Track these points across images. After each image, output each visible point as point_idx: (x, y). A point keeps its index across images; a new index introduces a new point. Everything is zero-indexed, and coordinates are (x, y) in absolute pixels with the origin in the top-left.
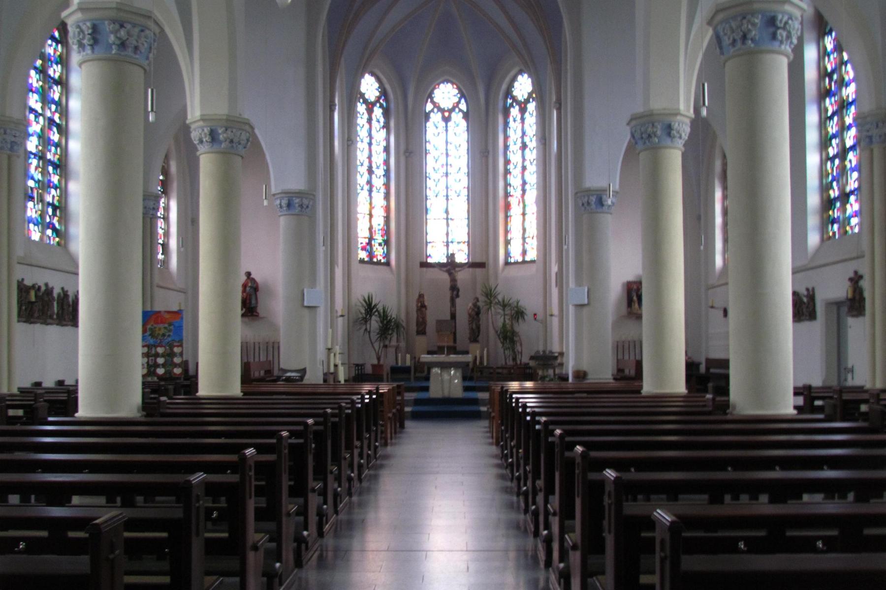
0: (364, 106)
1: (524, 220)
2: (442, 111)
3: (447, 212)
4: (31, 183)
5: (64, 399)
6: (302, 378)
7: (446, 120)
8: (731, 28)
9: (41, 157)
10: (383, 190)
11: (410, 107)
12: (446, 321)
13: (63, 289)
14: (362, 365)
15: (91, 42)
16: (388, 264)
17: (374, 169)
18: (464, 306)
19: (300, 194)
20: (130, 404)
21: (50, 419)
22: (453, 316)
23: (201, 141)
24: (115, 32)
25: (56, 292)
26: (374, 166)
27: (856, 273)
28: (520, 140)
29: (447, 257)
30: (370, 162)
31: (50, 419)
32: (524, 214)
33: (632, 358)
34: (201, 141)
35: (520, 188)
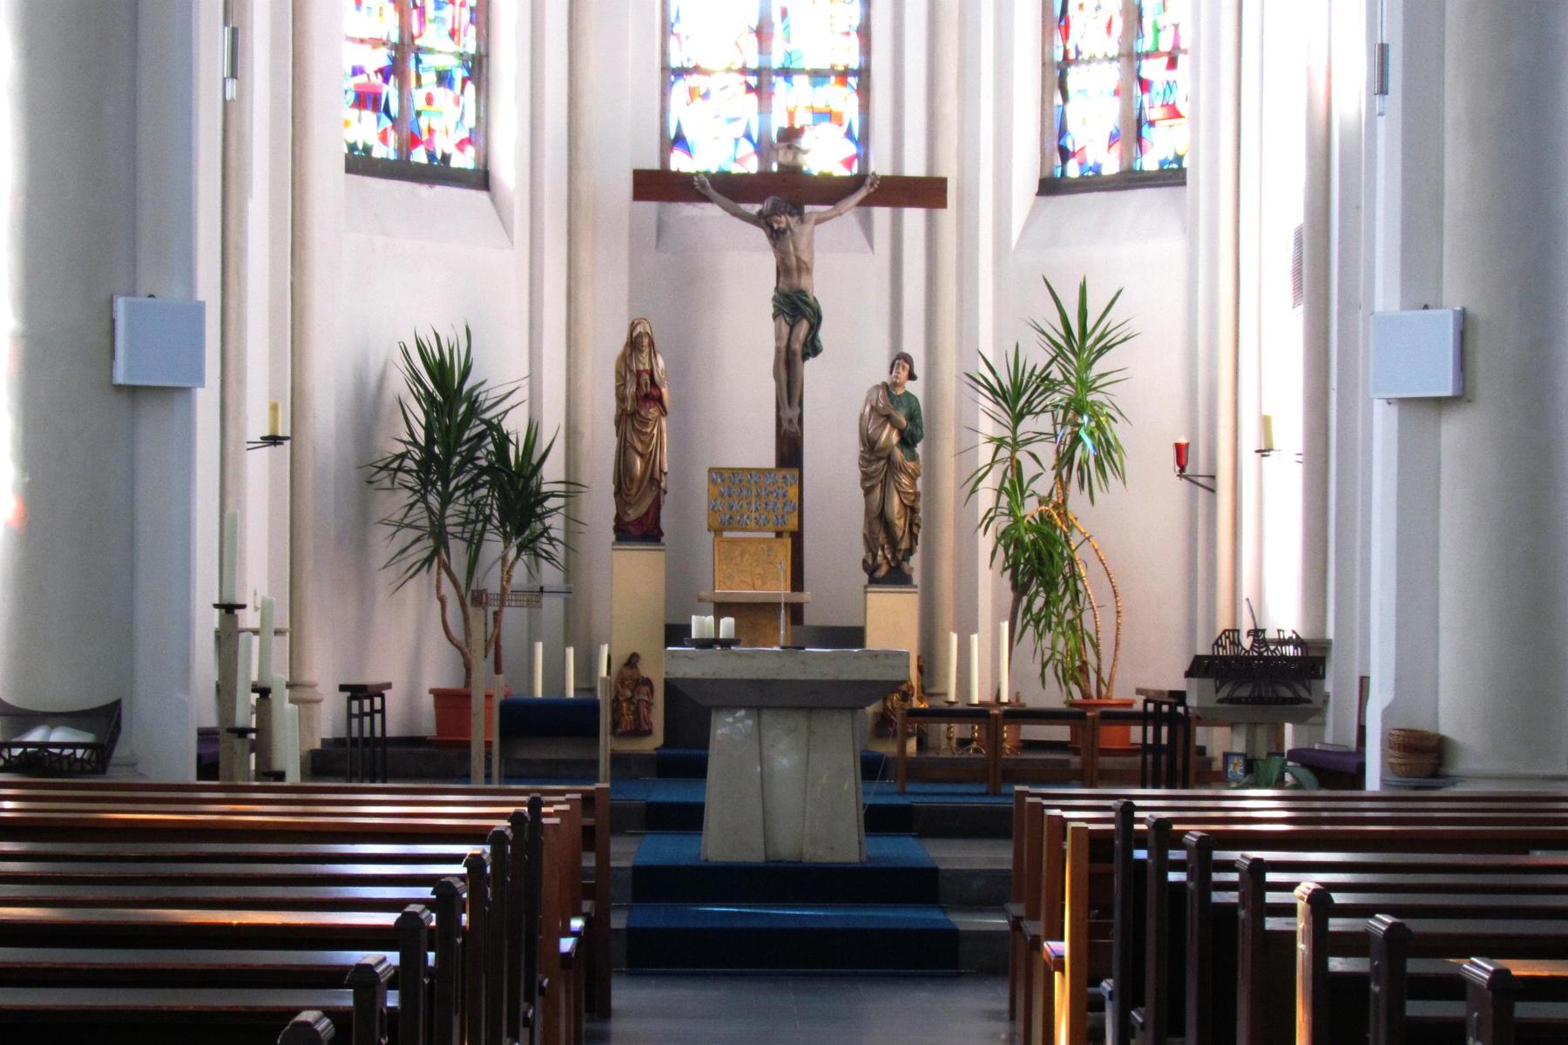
6: (102, 753)
12: (769, 471)
14: (377, 691)
16: (481, 179)
22: (790, 450)
29: (763, 149)
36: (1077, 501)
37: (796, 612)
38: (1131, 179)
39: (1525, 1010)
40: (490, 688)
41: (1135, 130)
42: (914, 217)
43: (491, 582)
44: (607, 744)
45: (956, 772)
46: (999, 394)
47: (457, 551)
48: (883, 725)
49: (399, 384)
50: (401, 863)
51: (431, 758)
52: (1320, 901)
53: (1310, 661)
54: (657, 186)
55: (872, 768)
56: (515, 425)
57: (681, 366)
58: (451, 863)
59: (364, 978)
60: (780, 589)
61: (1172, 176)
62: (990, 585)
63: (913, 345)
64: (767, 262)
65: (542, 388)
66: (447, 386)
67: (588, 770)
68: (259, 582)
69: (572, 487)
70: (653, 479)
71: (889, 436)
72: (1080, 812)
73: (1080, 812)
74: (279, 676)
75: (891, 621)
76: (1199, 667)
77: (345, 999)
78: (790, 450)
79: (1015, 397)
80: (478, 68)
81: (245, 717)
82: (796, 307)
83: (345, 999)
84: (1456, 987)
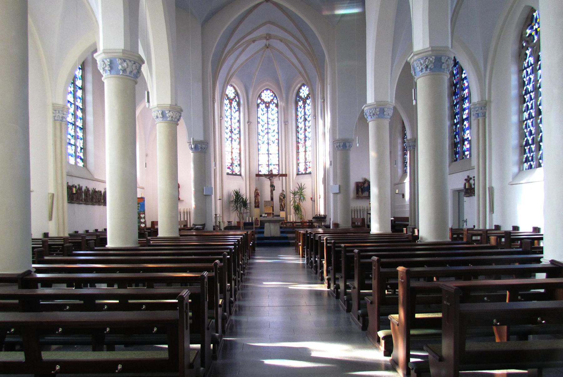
0: (228, 101)
1: (305, 154)
2: (265, 103)
3: (268, 150)
4: (69, 137)
5: (100, 238)
6: (203, 228)
7: (267, 107)
8: (421, 63)
9: (74, 124)
10: (238, 140)
11: (250, 101)
13: (87, 187)
15: (109, 69)
16: (240, 175)
17: (233, 130)
18: (277, 194)
19: (201, 142)
20: (131, 242)
21: (96, 248)
22: (272, 199)
23: (157, 117)
24: (121, 64)
25: (84, 188)
26: (233, 129)
27: (468, 176)
28: (303, 117)
29: (269, 172)
30: (231, 127)
31: (96, 248)
32: (305, 151)
33: (359, 217)
34: (157, 117)
35: (303, 139)
36: (301, 203)
37: (273, 214)
38: (306, 174)
39: (347, 249)
40: (242, 221)
41: (306, 169)
42: (284, 178)
43: (242, 211)
44: (254, 226)
45: (289, 228)
46: (293, 193)
47: (239, 209)
48: (282, 224)
49: (232, 194)
50: (234, 237)
51: (237, 228)
52: (326, 239)
53: (325, 217)
54: (258, 175)
55: (281, 228)
56: (244, 197)
57: (261, 191)
58: (239, 238)
59: (230, 249)
60: (272, 212)
61: (310, 173)
62: (292, 211)
63: (284, 189)
64: (269, 182)
65: (247, 193)
66: (237, 194)
67: (253, 229)
68: (219, 212)
69: (250, 203)
70: (258, 202)
71: (282, 197)
72: (302, 231)
73: (302, 231)
74: (221, 221)
75: (283, 214)
76: (314, 218)
77: (229, 251)
78: (272, 199)
79: (294, 194)
80: (240, 165)
81: (218, 224)
82: (272, 186)
83: (229, 251)
84: (340, 247)
